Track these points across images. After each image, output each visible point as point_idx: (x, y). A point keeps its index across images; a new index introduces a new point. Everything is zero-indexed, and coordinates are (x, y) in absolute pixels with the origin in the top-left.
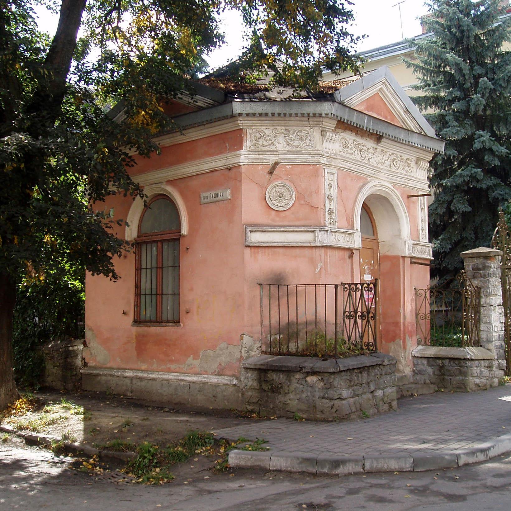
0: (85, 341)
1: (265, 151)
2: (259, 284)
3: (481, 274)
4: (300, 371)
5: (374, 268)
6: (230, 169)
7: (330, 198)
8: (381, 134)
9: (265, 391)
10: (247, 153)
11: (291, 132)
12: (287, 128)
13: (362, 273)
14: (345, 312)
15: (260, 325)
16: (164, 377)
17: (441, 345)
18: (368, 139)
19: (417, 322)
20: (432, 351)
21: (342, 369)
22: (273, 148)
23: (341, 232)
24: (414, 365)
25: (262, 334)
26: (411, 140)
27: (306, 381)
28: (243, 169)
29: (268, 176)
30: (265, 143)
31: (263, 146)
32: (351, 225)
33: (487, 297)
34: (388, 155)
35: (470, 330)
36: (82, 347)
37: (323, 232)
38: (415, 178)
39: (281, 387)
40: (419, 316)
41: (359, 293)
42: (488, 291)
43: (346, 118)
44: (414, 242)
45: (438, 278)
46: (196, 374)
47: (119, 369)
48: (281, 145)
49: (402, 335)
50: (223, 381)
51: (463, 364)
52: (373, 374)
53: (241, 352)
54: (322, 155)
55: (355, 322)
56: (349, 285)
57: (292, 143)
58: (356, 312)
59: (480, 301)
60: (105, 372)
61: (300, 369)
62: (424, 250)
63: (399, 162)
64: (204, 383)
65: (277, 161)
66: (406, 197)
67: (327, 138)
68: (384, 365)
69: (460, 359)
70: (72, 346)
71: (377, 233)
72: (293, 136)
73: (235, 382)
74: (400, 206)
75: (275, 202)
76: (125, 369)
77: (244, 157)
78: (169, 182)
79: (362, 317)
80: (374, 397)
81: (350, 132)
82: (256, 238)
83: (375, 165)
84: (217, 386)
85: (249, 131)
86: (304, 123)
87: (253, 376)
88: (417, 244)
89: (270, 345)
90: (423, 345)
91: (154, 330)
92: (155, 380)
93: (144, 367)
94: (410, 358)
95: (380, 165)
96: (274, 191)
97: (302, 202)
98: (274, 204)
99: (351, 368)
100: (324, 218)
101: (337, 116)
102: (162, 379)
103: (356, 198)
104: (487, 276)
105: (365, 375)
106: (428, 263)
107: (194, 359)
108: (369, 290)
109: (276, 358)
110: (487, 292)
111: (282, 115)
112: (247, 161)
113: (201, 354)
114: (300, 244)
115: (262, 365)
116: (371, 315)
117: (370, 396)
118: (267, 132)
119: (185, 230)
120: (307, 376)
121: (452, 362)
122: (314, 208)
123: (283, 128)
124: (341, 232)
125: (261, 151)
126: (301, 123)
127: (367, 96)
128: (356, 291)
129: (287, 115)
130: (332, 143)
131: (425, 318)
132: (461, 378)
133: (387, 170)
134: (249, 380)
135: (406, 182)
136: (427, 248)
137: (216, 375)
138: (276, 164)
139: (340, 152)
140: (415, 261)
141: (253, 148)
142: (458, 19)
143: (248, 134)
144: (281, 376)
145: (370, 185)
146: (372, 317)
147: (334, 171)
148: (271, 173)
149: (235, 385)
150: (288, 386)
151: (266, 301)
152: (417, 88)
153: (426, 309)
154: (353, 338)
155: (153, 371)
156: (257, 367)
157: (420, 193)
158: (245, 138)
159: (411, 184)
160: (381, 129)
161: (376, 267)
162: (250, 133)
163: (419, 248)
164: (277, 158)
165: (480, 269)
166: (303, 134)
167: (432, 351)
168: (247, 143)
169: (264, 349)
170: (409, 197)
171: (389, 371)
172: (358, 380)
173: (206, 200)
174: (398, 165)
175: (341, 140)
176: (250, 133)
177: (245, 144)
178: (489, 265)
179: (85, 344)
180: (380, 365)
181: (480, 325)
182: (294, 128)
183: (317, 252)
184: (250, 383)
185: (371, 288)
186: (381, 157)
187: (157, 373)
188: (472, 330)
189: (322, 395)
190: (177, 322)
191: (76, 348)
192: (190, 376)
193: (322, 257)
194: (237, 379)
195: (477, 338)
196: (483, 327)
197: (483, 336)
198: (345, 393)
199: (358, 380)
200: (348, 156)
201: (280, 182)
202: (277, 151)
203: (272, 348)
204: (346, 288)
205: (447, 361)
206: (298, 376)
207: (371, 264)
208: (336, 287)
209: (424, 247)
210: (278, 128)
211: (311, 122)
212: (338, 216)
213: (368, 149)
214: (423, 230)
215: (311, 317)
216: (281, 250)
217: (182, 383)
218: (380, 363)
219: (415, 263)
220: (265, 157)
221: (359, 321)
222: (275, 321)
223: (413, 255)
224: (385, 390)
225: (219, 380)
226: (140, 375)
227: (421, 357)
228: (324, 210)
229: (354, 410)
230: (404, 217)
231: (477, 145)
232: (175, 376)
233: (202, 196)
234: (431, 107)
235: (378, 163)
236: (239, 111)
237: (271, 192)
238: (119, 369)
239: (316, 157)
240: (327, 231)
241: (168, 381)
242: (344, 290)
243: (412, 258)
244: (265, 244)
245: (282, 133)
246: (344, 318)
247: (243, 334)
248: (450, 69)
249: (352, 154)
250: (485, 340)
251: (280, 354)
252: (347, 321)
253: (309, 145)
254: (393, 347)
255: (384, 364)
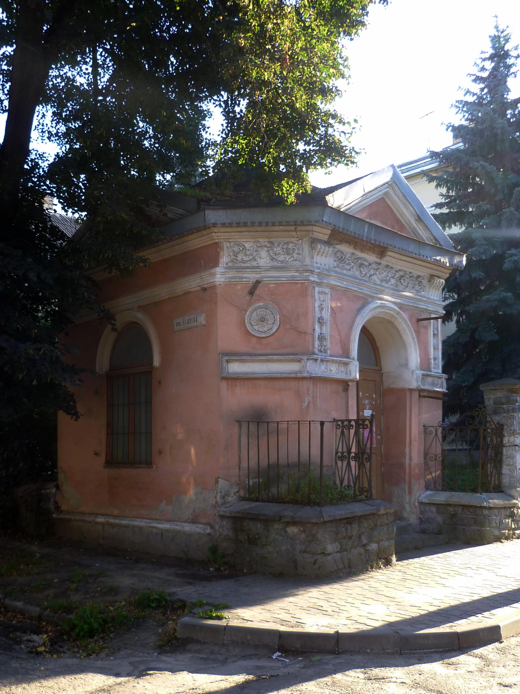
0: (58, 484)
1: (245, 268)
2: (237, 421)
3: (504, 408)
4: (279, 520)
5: (376, 403)
6: (205, 290)
7: (321, 321)
8: (385, 246)
9: (241, 541)
10: (223, 271)
11: (276, 244)
12: (271, 240)
13: (360, 408)
14: (337, 452)
15: (238, 467)
16: (136, 523)
17: (452, 489)
18: (370, 253)
19: (426, 463)
20: (442, 497)
21: (326, 519)
22: (254, 264)
23: (333, 361)
24: (422, 512)
25: (239, 477)
26: (422, 252)
27: (286, 532)
28: (219, 290)
29: (248, 297)
30: (245, 258)
31: (243, 261)
32: (346, 354)
33: (510, 436)
34: (394, 272)
35: (489, 473)
36: (54, 490)
37: (311, 361)
38: (428, 298)
39: (259, 538)
40: (428, 457)
41: (352, 431)
42: (513, 428)
43: (341, 225)
44: (423, 372)
45: (459, 415)
46: (169, 521)
47: (91, 514)
48: (264, 259)
49: (407, 478)
50: (196, 529)
51: (478, 511)
52: (366, 525)
53: (216, 497)
54: (312, 272)
55: (349, 464)
56: (342, 421)
57: (276, 257)
58: (349, 452)
59: (502, 441)
60: (77, 518)
61: (279, 519)
62: (436, 382)
63: (407, 280)
64: (178, 532)
65: (258, 279)
66: (414, 320)
67: (318, 250)
68: (379, 515)
69: (476, 507)
70: (45, 489)
71: (380, 363)
72: (278, 250)
73: (208, 531)
74: (408, 332)
75: (256, 327)
76: (97, 514)
77: (219, 276)
78: (142, 308)
79: (356, 458)
80: (367, 551)
81: (348, 245)
82: (235, 368)
83: (378, 282)
84: (189, 535)
85: (226, 245)
86: (290, 233)
87: (229, 525)
88: (428, 375)
89: (249, 490)
90: (432, 490)
91: (126, 472)
92: (127, 526)
93: (116, 512)
94: (417, 504)
95: (384, 284)
96: (254, 314)
97: (288, 327)
98: (257, 329)
99: (338, 518)
100: (313, 345)
101: (330, 224)
102: (134, 527)
103: (354, 321)
104: (511, 411)
105: (355, 526)
106: (441, 396)
107: (167, 504)
108: (365, 427)
109: (254, 504)
110: (510, 430)
111: (264, 224)
112: (223, 280)
113: (174, 499)
114: (284, 375)
115: (237, 512)
116: (366, 456)
117: (362, 550)
118: (247, 245)
119: (156, 362)
120: (287, 526)
121: (465, 510)
122: (302, 333)
123: (266, 240)
124: (333, 361)
125: (240, 268)
126: (287, 233)
127: (371, 201)
128: (349, 429)
129: (270, 224)
130: (320, 255)
131: (436, 460)
132: (476, 528)
133: (394, 290)
134: (224, 529)
135: (415, 303)
136: (440, 381)
137: (189, 522)
138: (258, 282)
139: (335, 267)
140: (424, 394)
141: (230, 264)
142: (491, 120)
143: (225, 248)
144: (259, 525)
145: (372, 306)
146: (366, 458)
147: (327, 290)
148: (251, 293)
149: (209, 534)
150: (266, 537)
151: (244, 440)
152: (439, 206)
153: (437, 449)
154: (345, 483)
155: (125, 517)
156: (233, 515)
157: (433, 316)
158: (221, 253)
159: (422, 306)
160: (384, 240)
161: (379, 402)
162: (227, 247)
163: (430, 379)
164: (259, 276)
165: (503, 404)
166: (291, 246)
167: (442, 497)
168: (224, 259)
169: (242, 493)
170: (419, 320)
171: (386, 521)
172: (346, 532)
173: (179, 327)
174: (406, 283)
175: (335, 254)
176: (227, 247)
177: (221, 261)
178: (515, 398)
179: (58, 487)
180: (374, 514)
181: (501, 467)
182: (280, 239)
183: (305, 385)
184: (226, 532)
185: (367, 425)
186: (385, 274)
187: (129, 519)
188: (492, 473)
189: (303, 548)
190: (149, 463)
191: (48, 491)
192: (162, 524)
193: (311, 392)
194: (212, 527)
195: (497, 483)
196: (505, 470)
197: (505, 480)
198: (330, 548)
199: (346, 532)
200: (345, 272)
201: (262, 304)
202: (258, 267)
203: (252, 494)
204: (339, 425)
205: (460, 509)
206: (276, 526)
207: (372, 398)
208: (322, 424)
209: (437, 379)
210: (260, 240)
211: (299, 233)
212: (331, 343)
213: (370, 264)
214: (435, 359)
215: (293, 458)
216: (263, 383)
217: (155, 531)
218: (375, 512)
219: (424, 397)
220: (244, 275)
221: (353, 463)
222: (253, 463)
223: (422, 387)
224: (381, 543)
225: (193, 528)
226: (112, 521)
227: (429, 504)
228: (313, 335)
229: (341, 566)
230: (412, 344)
231: (507, 265)
232: (147, 523)
233: (175, 323)
234: (455, 225)
235: (382, 281)
236: (213, 221)
237: (251, 317)
238: (91, 514)
239: (305, 274)
240: (316, 360)
241: (140, 528)
242: (337, 428)
243: (421, 391)
244: (245, 376)
245: (266, 246)
246: (336, 459)
247: (219, 478)
248: (480, 180)
249: (350, 270)
250: (507, 485)
251: (257, 500)
252: (339, 463)
253: (296, 260)
254: (396, 492)
255: (379, 513)
